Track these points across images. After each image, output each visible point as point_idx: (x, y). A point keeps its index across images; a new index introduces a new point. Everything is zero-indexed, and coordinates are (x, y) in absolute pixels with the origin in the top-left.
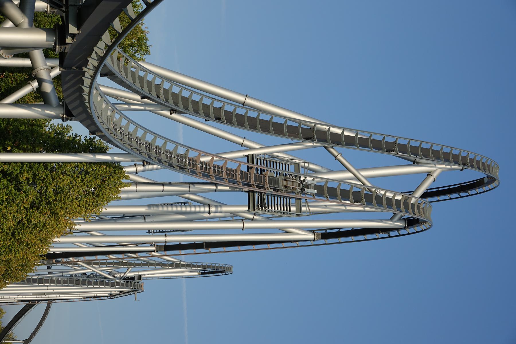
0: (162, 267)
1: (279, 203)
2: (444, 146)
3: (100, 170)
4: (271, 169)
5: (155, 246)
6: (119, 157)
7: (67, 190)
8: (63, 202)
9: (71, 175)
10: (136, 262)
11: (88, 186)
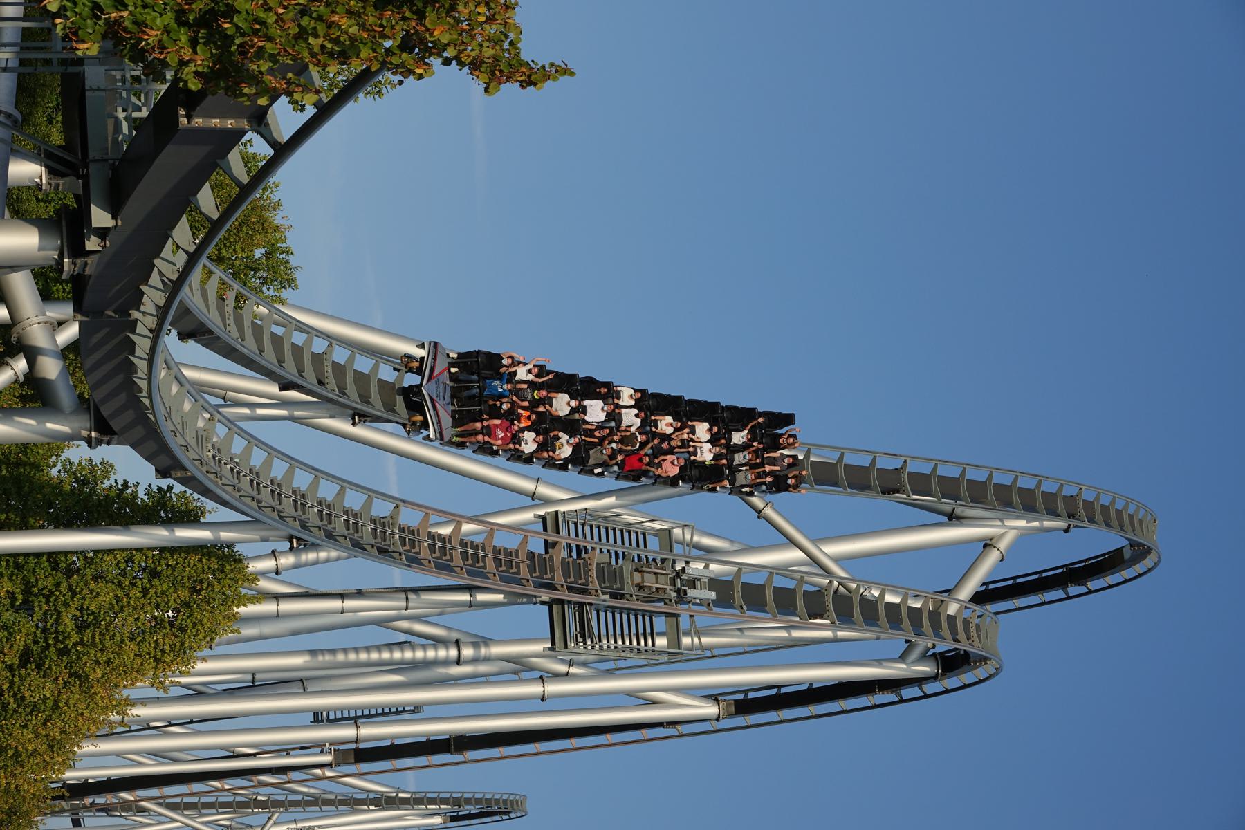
0: (355, 807)
1: (626, 631)
2: (1021, 473)
3: (186, 564)
4: (601, 544)
5: (331, 753)
6: (230, 531)
7: (108, 618)
8: (100, 646)
9: (116, 581)
10: (290, 798)
11: (158, 607)
